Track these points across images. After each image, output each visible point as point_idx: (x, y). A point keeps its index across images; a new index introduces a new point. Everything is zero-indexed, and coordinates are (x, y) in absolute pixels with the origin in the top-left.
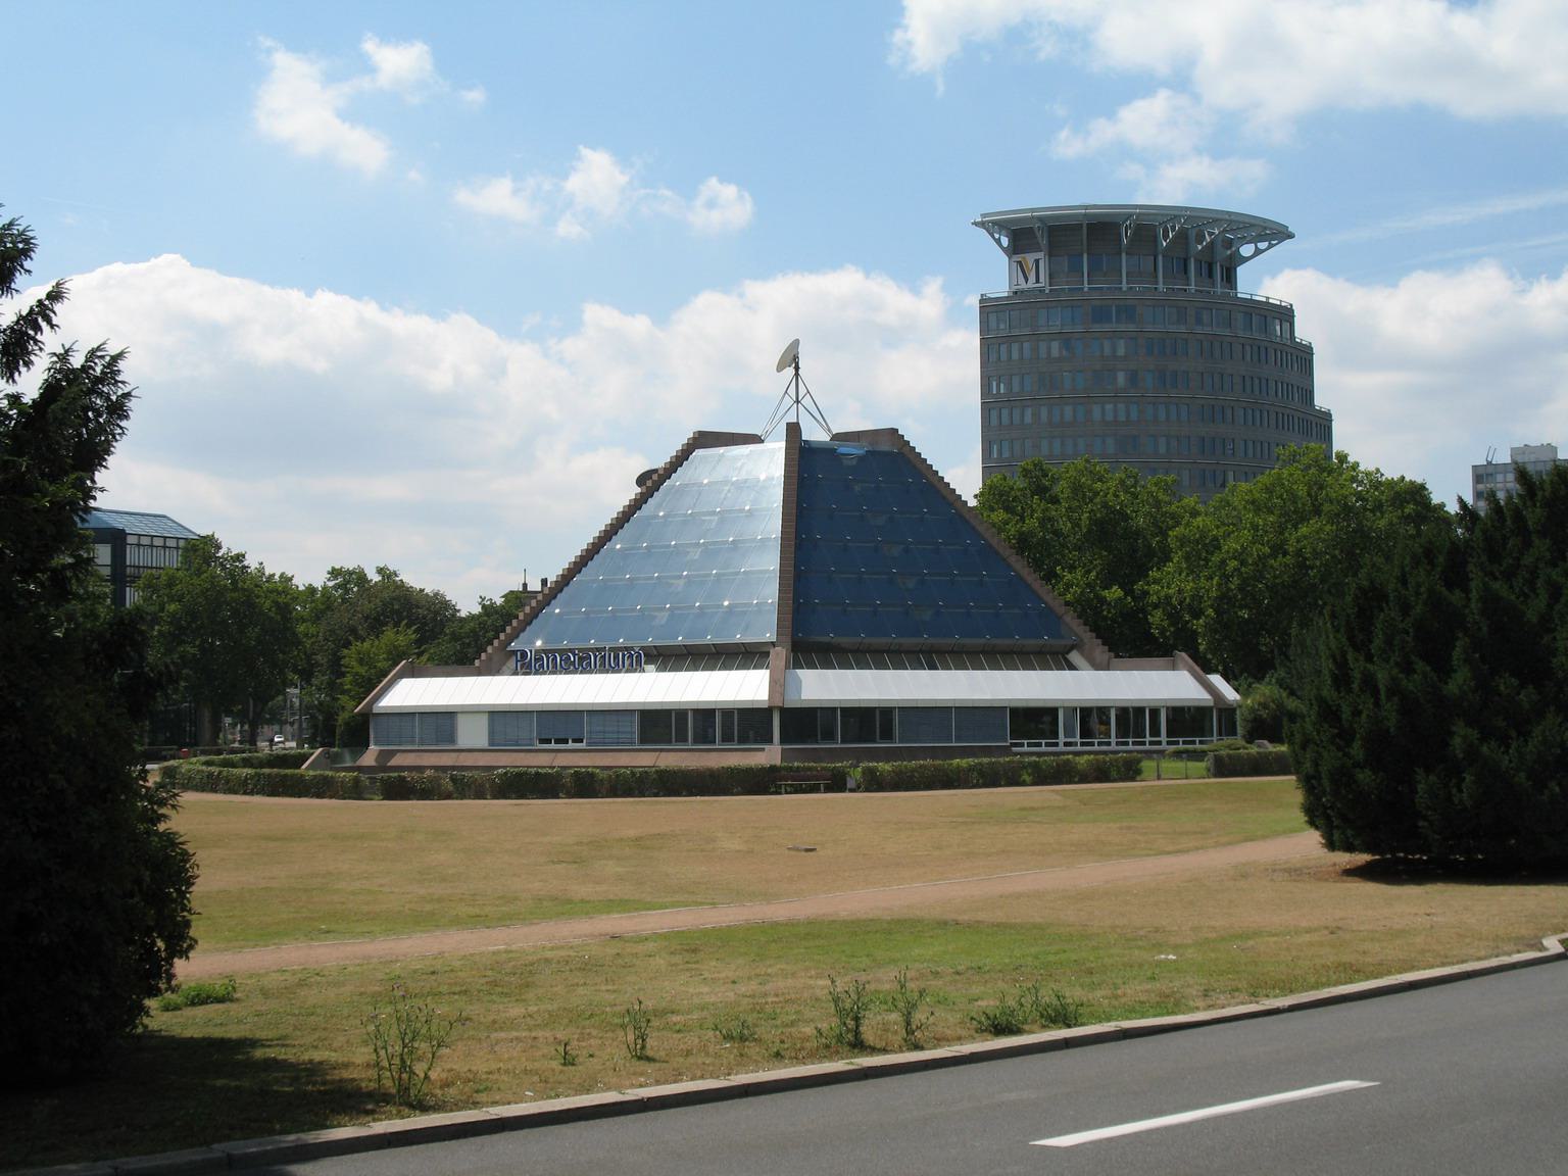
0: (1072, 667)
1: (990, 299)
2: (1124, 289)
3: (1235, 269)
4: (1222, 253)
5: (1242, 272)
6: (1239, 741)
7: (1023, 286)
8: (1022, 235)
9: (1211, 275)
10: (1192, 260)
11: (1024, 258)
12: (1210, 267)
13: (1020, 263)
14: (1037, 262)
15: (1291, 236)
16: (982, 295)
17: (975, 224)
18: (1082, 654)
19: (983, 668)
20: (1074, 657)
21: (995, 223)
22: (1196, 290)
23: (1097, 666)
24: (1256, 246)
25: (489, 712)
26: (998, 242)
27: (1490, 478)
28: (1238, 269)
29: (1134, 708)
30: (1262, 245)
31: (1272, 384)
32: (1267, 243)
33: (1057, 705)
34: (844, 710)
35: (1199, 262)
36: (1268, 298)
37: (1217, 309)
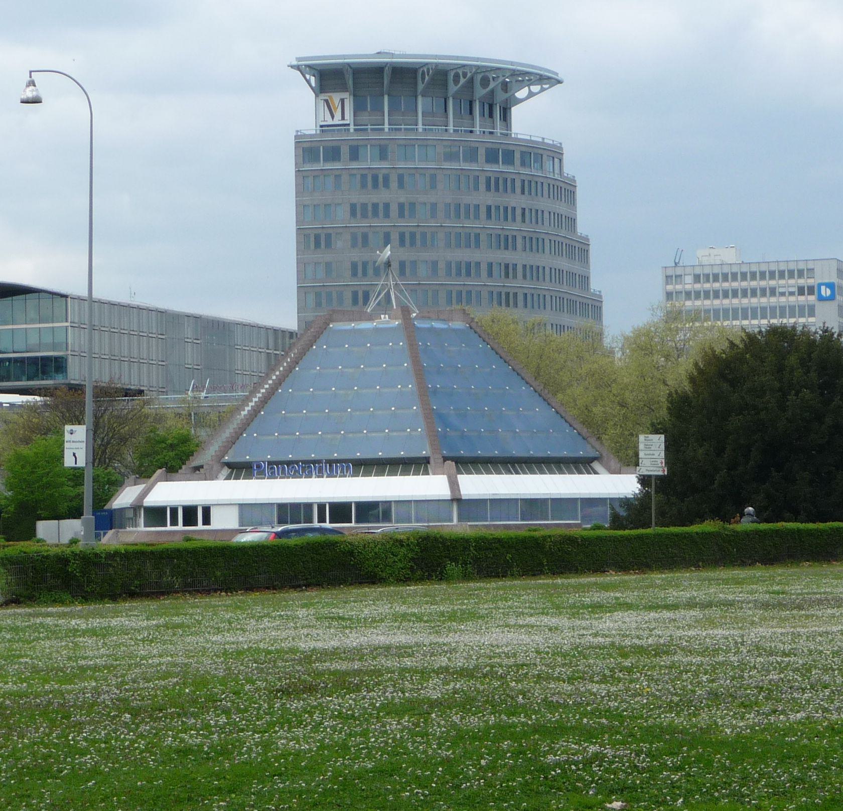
0: (596, 473)
1: (305, 135)
2: (420, 130)
4: (500, 96)
5: (516, 112)
6: (180, 527)
7: (330, 122)
8: (328, 78)
9: (491, 115)
12: (491, 107)
13: (326, 101)
14: (342, 101)
15: (559, 82)
16: (297, 131)
17: (292, 67)
19: (471, 473)
20: (596, 465)
21: (309, 66)
26: (308, 82)
27: (679, 280)
28: (513, 109)
30: (535, 88)
31: (546, 215)
33: (194, 504)
34: (553, 500)
36: (543, 139)
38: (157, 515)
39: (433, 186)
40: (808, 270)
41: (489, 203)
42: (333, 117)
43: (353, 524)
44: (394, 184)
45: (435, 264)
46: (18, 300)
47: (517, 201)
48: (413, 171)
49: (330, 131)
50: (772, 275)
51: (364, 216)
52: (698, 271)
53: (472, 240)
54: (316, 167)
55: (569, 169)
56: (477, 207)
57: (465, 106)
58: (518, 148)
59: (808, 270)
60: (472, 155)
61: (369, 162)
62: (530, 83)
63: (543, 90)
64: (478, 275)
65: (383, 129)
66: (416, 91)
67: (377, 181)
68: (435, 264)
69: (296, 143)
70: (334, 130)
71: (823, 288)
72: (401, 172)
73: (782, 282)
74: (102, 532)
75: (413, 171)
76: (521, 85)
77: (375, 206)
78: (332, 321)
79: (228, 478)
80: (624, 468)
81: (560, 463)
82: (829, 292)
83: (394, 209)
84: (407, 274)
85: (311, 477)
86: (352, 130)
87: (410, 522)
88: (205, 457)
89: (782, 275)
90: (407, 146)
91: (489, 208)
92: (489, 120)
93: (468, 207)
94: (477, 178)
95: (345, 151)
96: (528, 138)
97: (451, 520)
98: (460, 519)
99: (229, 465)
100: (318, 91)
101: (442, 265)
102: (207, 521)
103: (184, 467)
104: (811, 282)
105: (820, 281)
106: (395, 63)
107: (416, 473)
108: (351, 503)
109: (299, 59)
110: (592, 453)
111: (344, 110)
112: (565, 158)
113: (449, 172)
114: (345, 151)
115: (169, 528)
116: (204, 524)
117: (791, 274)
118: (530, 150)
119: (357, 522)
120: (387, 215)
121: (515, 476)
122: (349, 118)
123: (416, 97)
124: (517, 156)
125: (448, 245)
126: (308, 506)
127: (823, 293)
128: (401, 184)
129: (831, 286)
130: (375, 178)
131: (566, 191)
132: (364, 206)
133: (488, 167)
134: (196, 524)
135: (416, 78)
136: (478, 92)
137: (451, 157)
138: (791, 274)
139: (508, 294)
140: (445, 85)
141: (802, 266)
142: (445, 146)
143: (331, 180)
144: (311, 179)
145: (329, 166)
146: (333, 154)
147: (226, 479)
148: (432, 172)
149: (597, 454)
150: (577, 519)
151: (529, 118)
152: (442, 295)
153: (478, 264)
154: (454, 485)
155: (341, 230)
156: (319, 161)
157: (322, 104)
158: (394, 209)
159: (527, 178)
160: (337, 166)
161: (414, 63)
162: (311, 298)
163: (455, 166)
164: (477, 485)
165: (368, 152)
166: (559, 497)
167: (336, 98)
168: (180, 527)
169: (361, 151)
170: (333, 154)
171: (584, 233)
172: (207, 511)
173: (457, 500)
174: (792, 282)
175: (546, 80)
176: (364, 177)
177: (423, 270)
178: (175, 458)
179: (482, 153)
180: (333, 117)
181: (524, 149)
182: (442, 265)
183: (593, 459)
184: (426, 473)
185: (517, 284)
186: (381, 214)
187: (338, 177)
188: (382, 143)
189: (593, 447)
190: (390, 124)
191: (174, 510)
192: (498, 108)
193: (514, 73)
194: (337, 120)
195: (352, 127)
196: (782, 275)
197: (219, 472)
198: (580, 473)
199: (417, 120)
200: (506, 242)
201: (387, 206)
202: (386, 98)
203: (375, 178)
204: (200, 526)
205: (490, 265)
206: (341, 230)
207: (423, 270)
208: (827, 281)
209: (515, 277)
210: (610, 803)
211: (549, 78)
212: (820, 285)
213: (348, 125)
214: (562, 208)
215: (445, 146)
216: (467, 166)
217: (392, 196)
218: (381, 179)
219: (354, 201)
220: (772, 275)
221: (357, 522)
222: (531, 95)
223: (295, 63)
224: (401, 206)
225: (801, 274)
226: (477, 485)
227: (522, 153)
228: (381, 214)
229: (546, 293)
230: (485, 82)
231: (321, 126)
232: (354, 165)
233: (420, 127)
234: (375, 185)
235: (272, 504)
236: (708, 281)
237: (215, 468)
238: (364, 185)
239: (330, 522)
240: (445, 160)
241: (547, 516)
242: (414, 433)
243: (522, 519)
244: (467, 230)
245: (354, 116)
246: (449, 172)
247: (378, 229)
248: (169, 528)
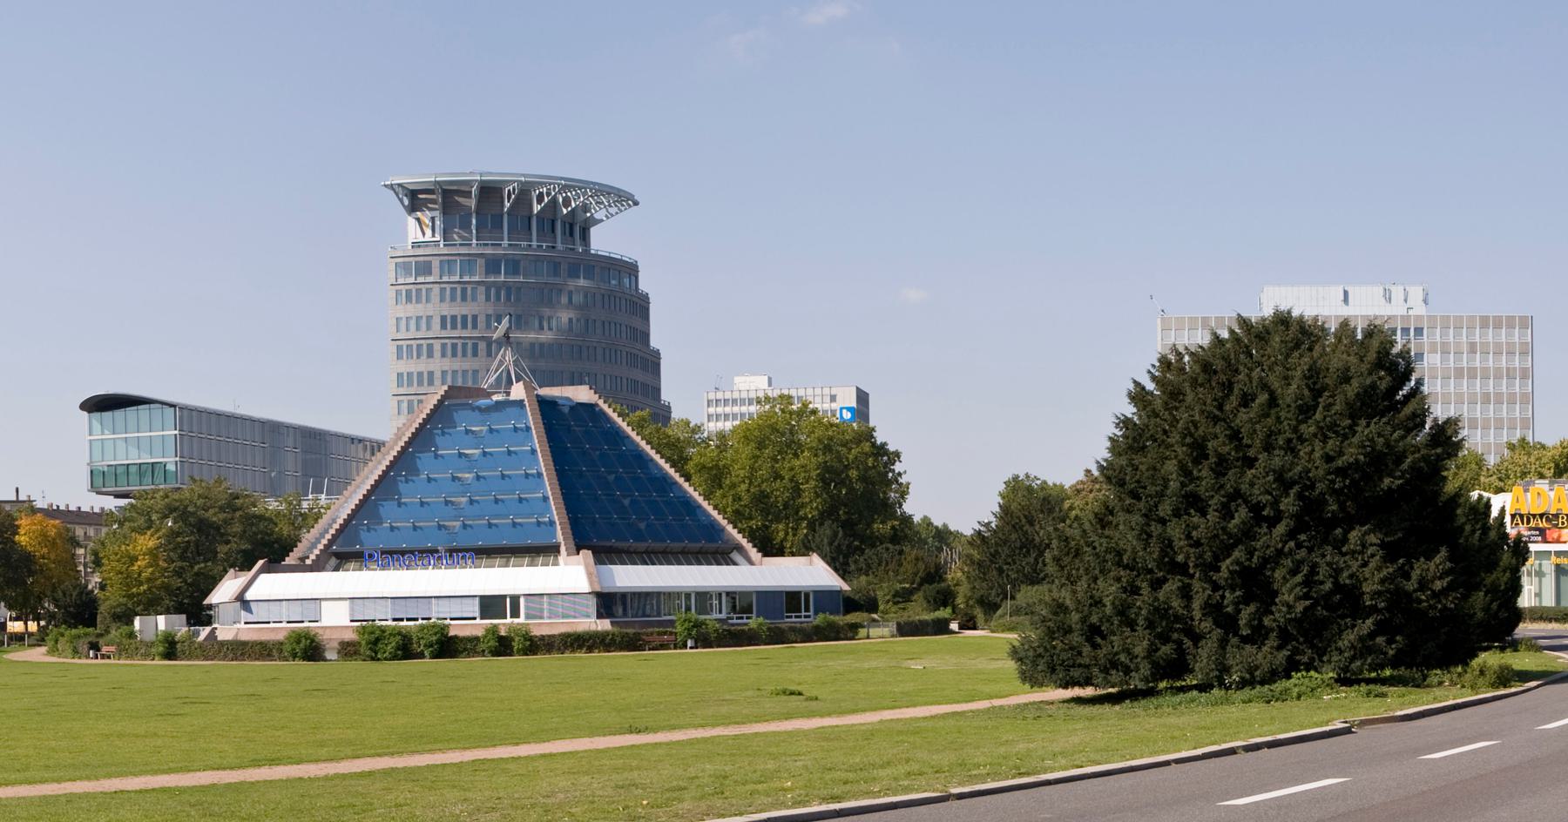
0: (735, 564)
5: (594, 232)
7: (421, 239)
9: (571, 234)
12: (571, 226)
14: (433, 219)
15: (636, 203)
26: (401, 201)
43: (509, 620)
46: (131, 412)
51: (454, 327)
55: (644, 286)
57: (547, 226)
79: (336, 569)
88: (313, 541)
112: (641, 275)
121: (715, 567)
178: (271, 549)
191: (515, 600)
197: (326, 562)
198: (719, 564)
201: (431, 374)
210: (132, 505)
214: (636, 322)
233: (506, 242)
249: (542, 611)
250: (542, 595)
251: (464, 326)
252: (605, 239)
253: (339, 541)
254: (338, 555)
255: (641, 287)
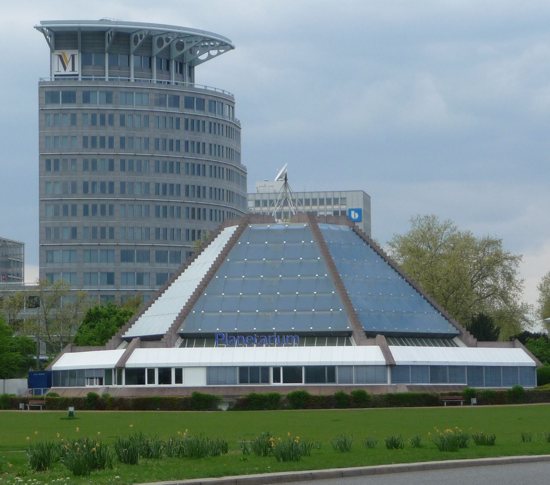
0: (457, 346)
2: (107, 80)
3: (194, 67)
5: (198, 70)
6: (156, 385)
7: (63, 72)
8: (62, 38)
10: (155, 58)
11: (63, 53)
13: (60, 56)
14: (73, 56)
15: (232, 48)
16: (41, 79)
17: (37, 28)
18: (461, 339)
20: (456, 340)
22: (157, 82)
23: (469, 345)
24: (218, 51)
25: (207, 367)
28: (195, 67)
29: (308, 368)
30: (213, 52)
32: (217, 51)
33: (169, 366)
35: (159, 61)
36: (223, 91)
37: (100, 92)
38: (136, 375)
39: (147, 124)
40: (341, 198)
41: (187, 139)
42: (65, 68)
43: (303, 384)
44: (117, 122)
45: (148, 185)
47: (206, 138)
48: (131, 113)
49: (69, 79)
50: (314, 202)
52: (258, 197)
53: (172, 167)
54: (56, 107)
56: (178, 142)
58: (208, 97)
59: (341, 198)
60: (175, 101)
61: (98, 104)
62: (214, 47)
63: (219, 53)
64: (179, 194)
65: (104, 79)
66: (129, 51)
67: (101, 119)
68: (148, 185)
69: (40, 88)
70: (65, 79)
71: (353, 212)
72: (122, 113)
73: (322, 207)
74: (42, 389)
75: (131, 113)
76: (206, 49)
77: (103, 139)
78: (250, 223)
79: (183, 346)
80: (480, 343)
81: (433, 338)
82: (357, 216)
83: (117, 141)
84: (126, 193)
85: (262, 346)
86: (80, 80)
87: (351, 382)
89: (322, 202)
90: (129, 92)
91: (187, 143)
92: (180, 75)
93: (171, 141)
94: (178, 120)
95: (79, 95)
96: (214, 90)
97: (386, 382)
98: (393, 381)
99: (183, 336)
100: (53, 48)
101: (117, 186)
102: (179, 379)
103: (113, 337)
104: (343, 207)
105: (351, 207)
106: (83, 27)
107: (341, 344)
108: (301, 367)
109: (42, 22)
110: (454, 331)
111: (74, 64)
112: (236, 106)
113: (157, 114)
114: (79, 95)
115: (147, 385)
116: (176, 382)
117: (329, 202)
118: (214, 99)
119: (307, 382)
120: (111, 146)
121: (422, 347)
122: (78, 70)
123: (129, 56)
124: (207, 103)
125: (157, 170)
126: (265, 369)
127: (353, 216)
128: (122, 123)
129: (358, 211)
130: (103, 118)
131: (233, 130)
132: (94, 139)
133: (186, 112)
134: (144, 384)
135: (129, 41)
136: (170, 53)
137: (161, 102)
138: (329, 202)
139: (193, 209)
140: (151, 47)
141: (337, 196)
142: (155, 94)
143: (67, 119)
144: (52, 116)
145: (67, 106)
146: (69, 97)
147: (180, 347)
148: (147, 114)
149: (458, 332)
150: (463, 381)
151: (208, 74)
152: (152, 209)
153: (179, 186)
154: (387, 354)
155: (76, 157)
156: (59, 102)
157: (56, 59)
158: (117, 141)
159: (213, 121)
160: (73, 106)
161: (129, 29)
162: (51, 211)
163: (163, 109)
164: (405, 354)
165: (98, 96)
166: (319, 365)
167: (68, 54)
168: (156, 385)
169: (92, 96)
170: (69, 97)
171: (244, 165)
172: (179, 372)
173: (392, 366)
174: (329, 207)
175: (225, 46)
176: (94, 116)
177: (138, 190)
179: (182, 100)
180: (65, 68)
181: (211, 98)
182: (152, 186)
183: (454, 336)
184: (349, 344)
185: (206, 202)
186: (107, 145)
187: (74, 116)
188: (109, 90)
189: (454, 326)
190: (109, 76)
191: (151, 371)
192: (186, 67)
193: (205, 39)
194: (69, 71)
195: (80, 77)
196: (322, 202)
199: (105, 72)
200: (197, 169)
201: (111, 139)
202: (107, 55)
203: (103, 118)
204: (173, 384)
205: (187, 187)
206: (76, 157)
207: (138, 190)
208: (356, 207)
209: (204, 196)
211: (227, 44)
212: (350, 210)
213: (77, 75)
215: (155, 94)
216: (171, 110)
217: (115, 131)
218: (107, 118)
219: (86, 134)
220: (314, 202)
221: (307, 382)
222: (210, 57)
223: (39, 25)
224: (122, 139)
225: (336, 201)
226: (405, 354)
227: (210, 101)
228: (107, 145)
229: (216, 208)
230: (160, 42)
231: (55, 76)
232: (86, 106)
234: (103, 123)
235: (235, 367)
236: (265, 205)
237: (173, 338)
238: (94, 123)
239: (284, 383)
240: (156, 104)
241: (409, 380)
242: (335, 313)
243: (431, 382)
244: (171, 160)
245: (82, 68)
246: (157, 114)
247: (104, 157)
248: (147, 385)
249: (351, 377)
250: (352, 366)
251: (103, 145)
252: (208, 74)
253: (183, 325)
254: (183, 336)
255: (236, 116)
